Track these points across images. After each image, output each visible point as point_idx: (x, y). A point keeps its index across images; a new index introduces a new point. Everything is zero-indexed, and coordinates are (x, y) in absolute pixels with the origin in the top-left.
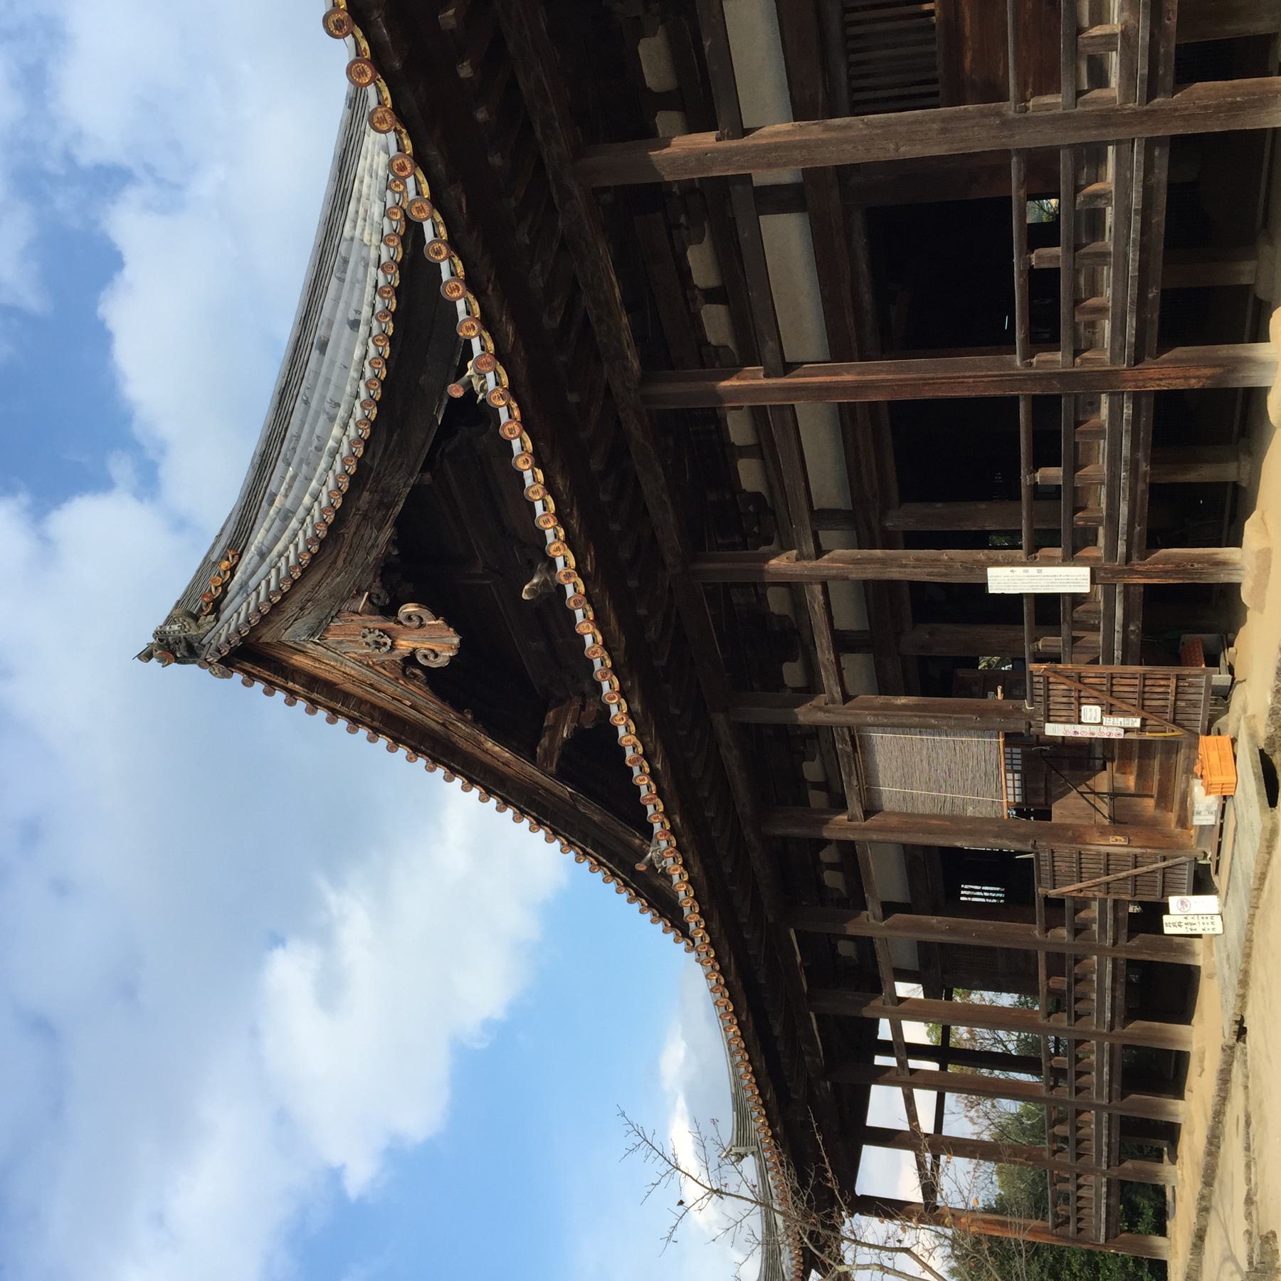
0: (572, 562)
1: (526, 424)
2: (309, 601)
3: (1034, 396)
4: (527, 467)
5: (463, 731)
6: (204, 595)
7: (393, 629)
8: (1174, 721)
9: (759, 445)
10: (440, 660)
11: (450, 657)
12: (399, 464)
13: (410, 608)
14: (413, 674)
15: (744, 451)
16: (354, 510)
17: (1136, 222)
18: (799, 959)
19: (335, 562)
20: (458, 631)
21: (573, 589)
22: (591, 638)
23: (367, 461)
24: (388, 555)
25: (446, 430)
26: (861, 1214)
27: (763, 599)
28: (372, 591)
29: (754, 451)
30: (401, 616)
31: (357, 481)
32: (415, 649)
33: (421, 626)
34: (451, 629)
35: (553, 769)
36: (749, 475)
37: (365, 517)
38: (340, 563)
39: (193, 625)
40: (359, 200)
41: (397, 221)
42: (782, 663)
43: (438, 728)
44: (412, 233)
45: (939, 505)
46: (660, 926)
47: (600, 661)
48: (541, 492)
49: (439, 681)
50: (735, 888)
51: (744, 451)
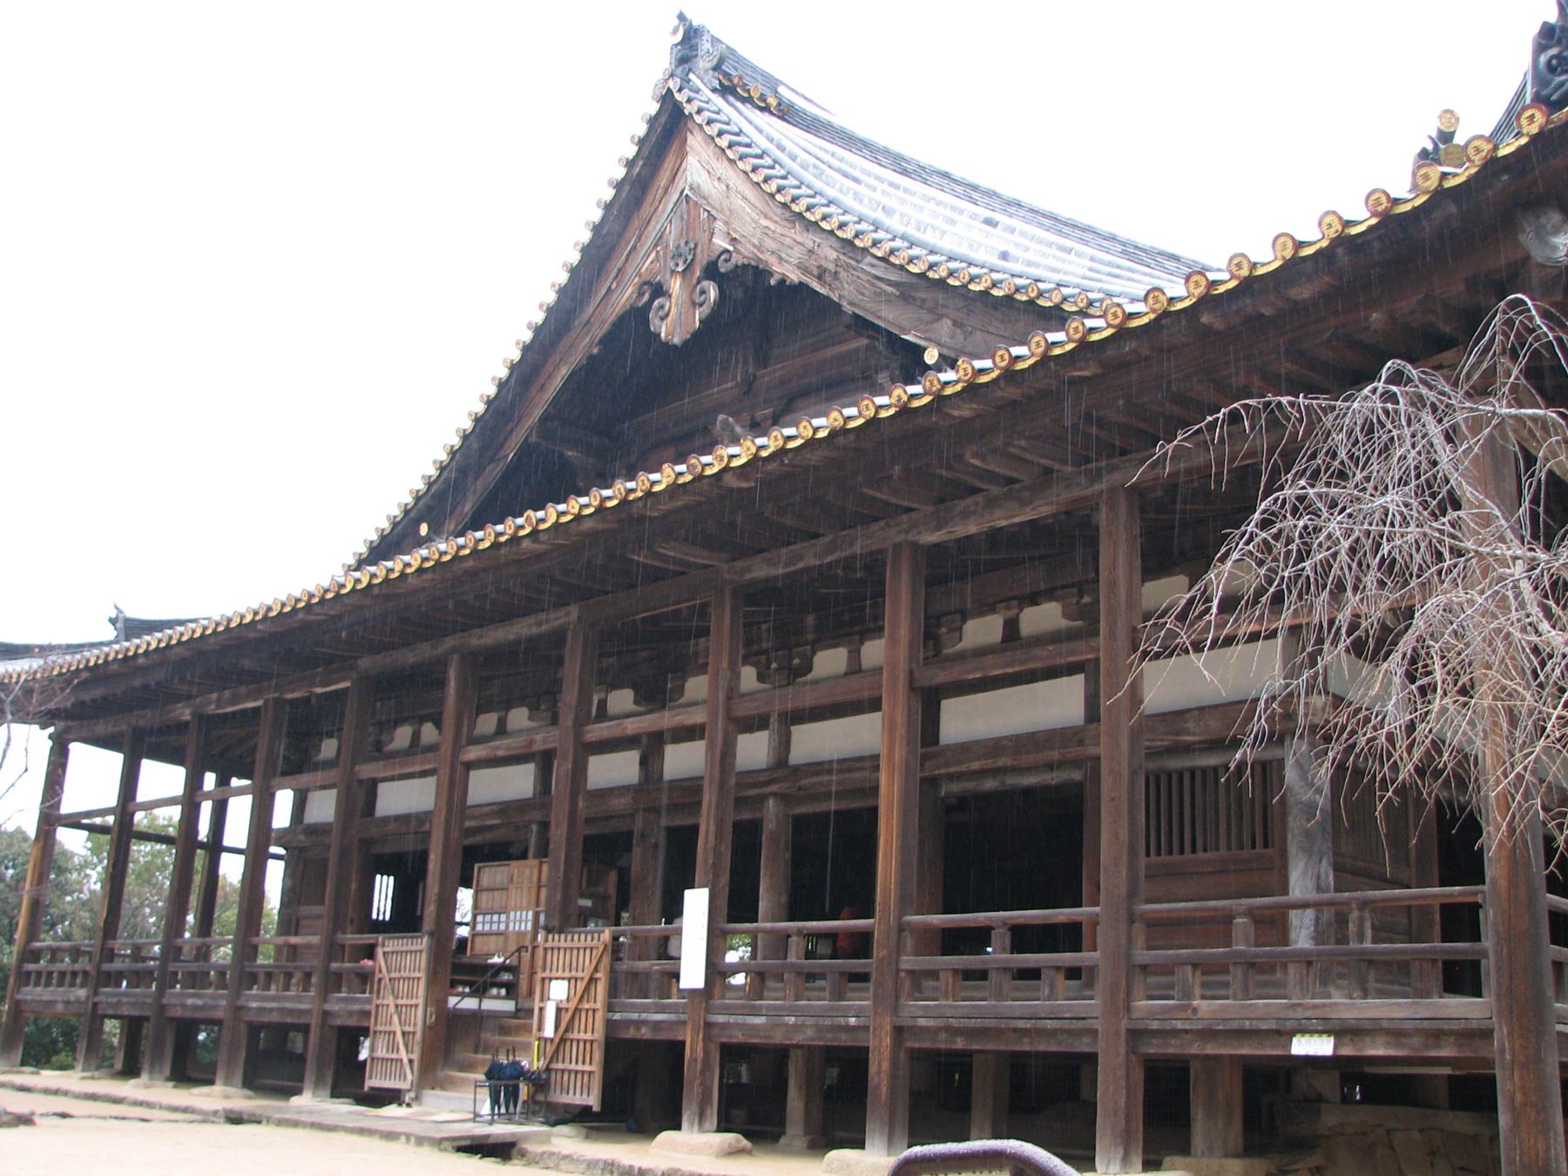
2: (727, 187)
3: (873, 933)
5: (583, 345)
6: (741, 78)
10: (657, 322)
11: (659, 335)
12: (863, 291)
13: (713, 293)
14: (644, 294)
15: (855, 656)
16: (818, 240)
18: (319, 690)
20: (686, 343)
21: (711, 463)
22: (662, 478)
24: (771, 274)
25: (894, 342)
26: (52, 748)
30: (705, 283)
32: (670, 296)
33: (694, 304)
38: (765, 222)
39: (710, 65)
42: (634, 687)
43: (585, 317)
47: (637, 486)
51: (855, 656)
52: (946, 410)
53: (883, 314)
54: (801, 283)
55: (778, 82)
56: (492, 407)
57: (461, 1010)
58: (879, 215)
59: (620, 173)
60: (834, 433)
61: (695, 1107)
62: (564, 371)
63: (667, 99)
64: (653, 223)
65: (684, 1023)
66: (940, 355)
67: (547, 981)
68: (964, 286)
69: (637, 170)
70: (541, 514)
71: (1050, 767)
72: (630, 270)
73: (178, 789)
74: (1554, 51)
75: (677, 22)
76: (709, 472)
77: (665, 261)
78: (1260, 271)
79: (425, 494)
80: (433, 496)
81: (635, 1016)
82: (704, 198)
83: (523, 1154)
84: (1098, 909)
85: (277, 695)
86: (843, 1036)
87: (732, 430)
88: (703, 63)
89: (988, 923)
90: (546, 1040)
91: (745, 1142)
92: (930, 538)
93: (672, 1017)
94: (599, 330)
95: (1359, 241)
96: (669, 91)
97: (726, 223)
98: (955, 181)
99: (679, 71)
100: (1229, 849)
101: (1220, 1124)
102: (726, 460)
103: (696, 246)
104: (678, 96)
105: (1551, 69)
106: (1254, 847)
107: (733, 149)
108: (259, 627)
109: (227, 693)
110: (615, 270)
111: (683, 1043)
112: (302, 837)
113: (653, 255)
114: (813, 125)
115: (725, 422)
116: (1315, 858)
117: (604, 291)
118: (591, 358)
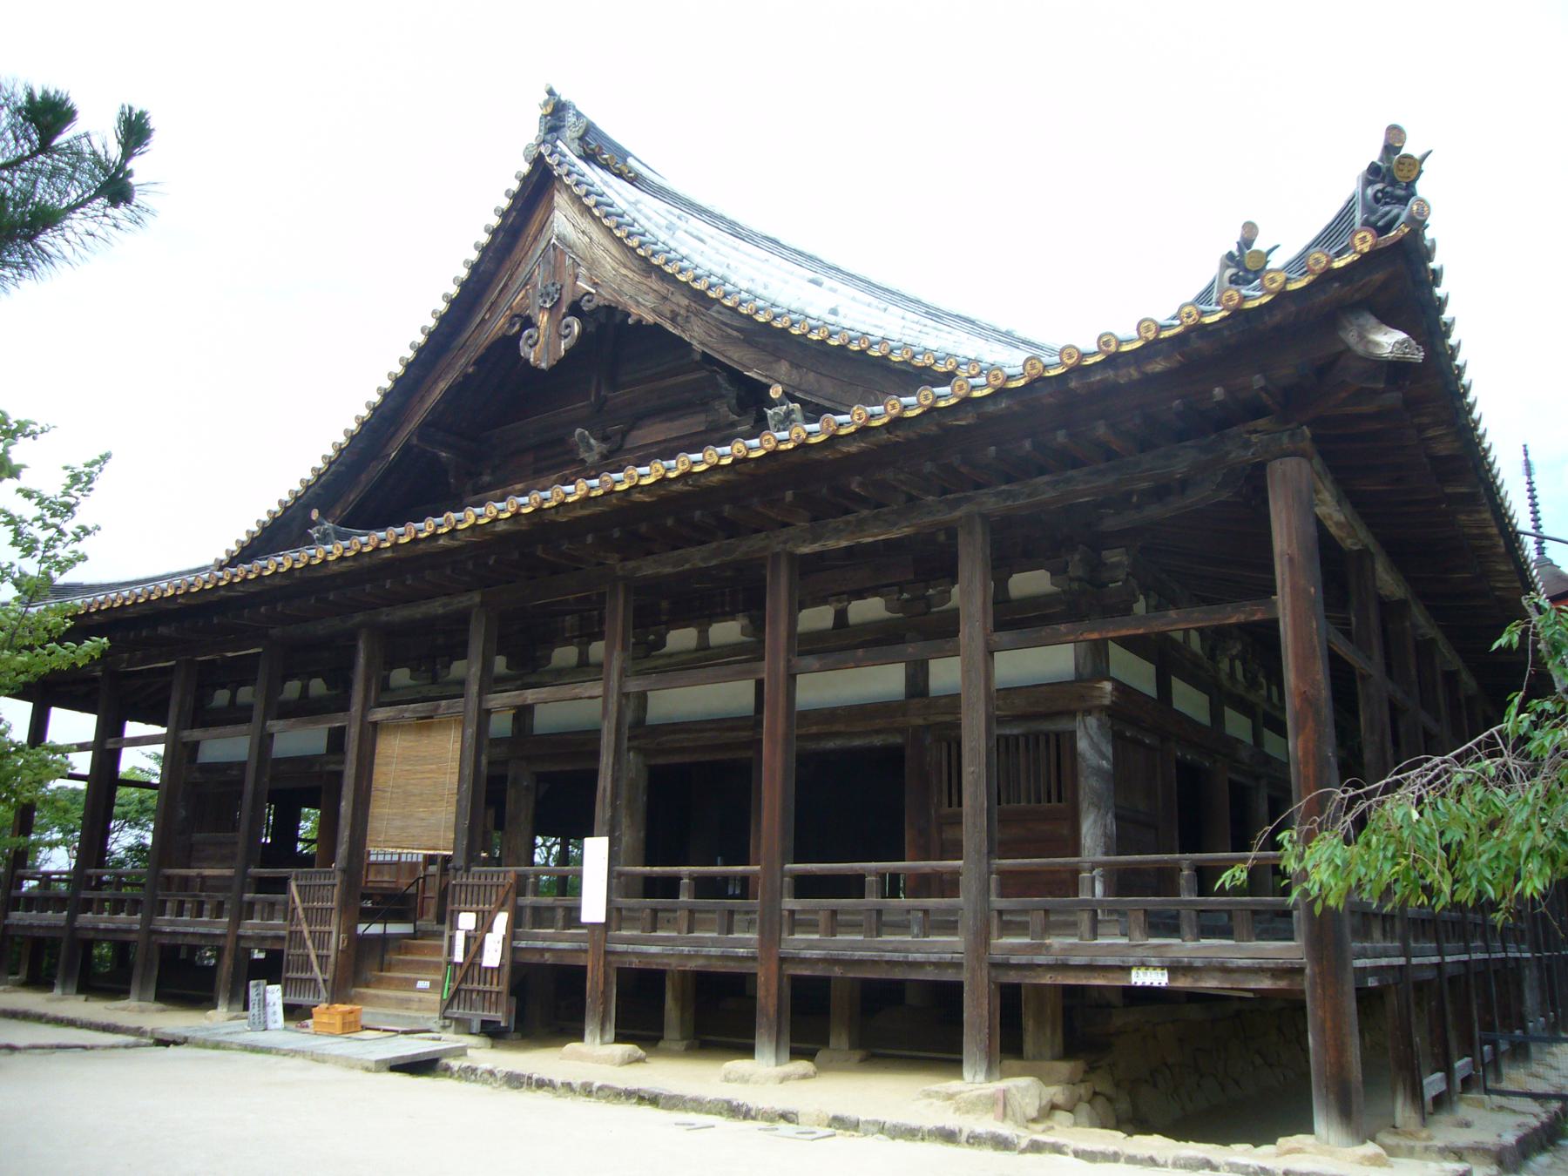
0: (644, 482)
1: (773, 455)
2: (591, 239)
4: (735, 451)
5: (461, 364)
7: (560, 310)
8: (458, 991)
9: (708, 648)
10: (527, 349)
12: (712, 333)
14: (514, 325)
16: (672, 289)
17: (896, 956)
18: (230, 654)
19: (625, 266)
20: (552, 368)
23: (716, 307)
24: (628, 315)
25: (736, 377)
27: (567, 642)
28: (596, 296)
29: (704, 644)
30: (569, 319)
31: (701, 297)
34: (555, 363)
35: (415, 441)
36: (681, 639)
37: (665, 298)
38: (624, 271)
39: (576, 135)
40: (935, 328)
41: (923, 361)
43: (461, 340)
44: (948, 378)
45: (645, 798)
46: (255, 528)
48: (710, 461)
49: (508, 344)
50: (313, 601)
51: (703, 635)
52: (839, 447)
53: (729, 354)
54: (656, 324)
55: (629, 154)
56: (377, 413)
57: (368, 935)
58: (727, 273)
59: (495, 221)
60: (736, 462)
61: (597, 1020)
62: (442, 386)
63: (538, 163)
64: (523, 265)
65: (586, 951)
66: (783, 391)
67: (456, 913)
68: (804, 335)
69: (511, 220)
70: (460, 515)
71: (878, 732)
72: (503, 305)
73: (89, 735)
74: (1379, 186)
75: (547, 97)
76: (619, 488)
77: (534, 297)
78: (1125, 348)
79: (314, 484)
80: (322, 486)
81: (539, 944)
82: (570, 247)
83: (447, 1069)
84: (960, 863)
85: (189, 657)
86: (732, 964)
87: (588, 442)
88: (571, 132)
89: (861, 872)
90: (456, 964)
91: (640, 1052)
92: (806, 549)
93: (574, 945)
94: (473, 353)
95: (1210, 328)
96: (541, 156)
97: (588, 269)
98: (784, 247)
99: (549, 137)
100: (1029, 802)
101: (1048, 1033)
102: (636, 479)
103: (562, 286)
104: (548, 159)
105: (1376, 199)
106: (1049, 801)
107: (590, 208)
108: (180, 600)
109: (139, 654)
110: (489, 304)
111: (585, 967)
112: (197, 775)
113: (523, 292)
114: (660, 192)
115: (582, 435)
116: (1102, 811)
117: (478, 320)
118: (467, 376)
